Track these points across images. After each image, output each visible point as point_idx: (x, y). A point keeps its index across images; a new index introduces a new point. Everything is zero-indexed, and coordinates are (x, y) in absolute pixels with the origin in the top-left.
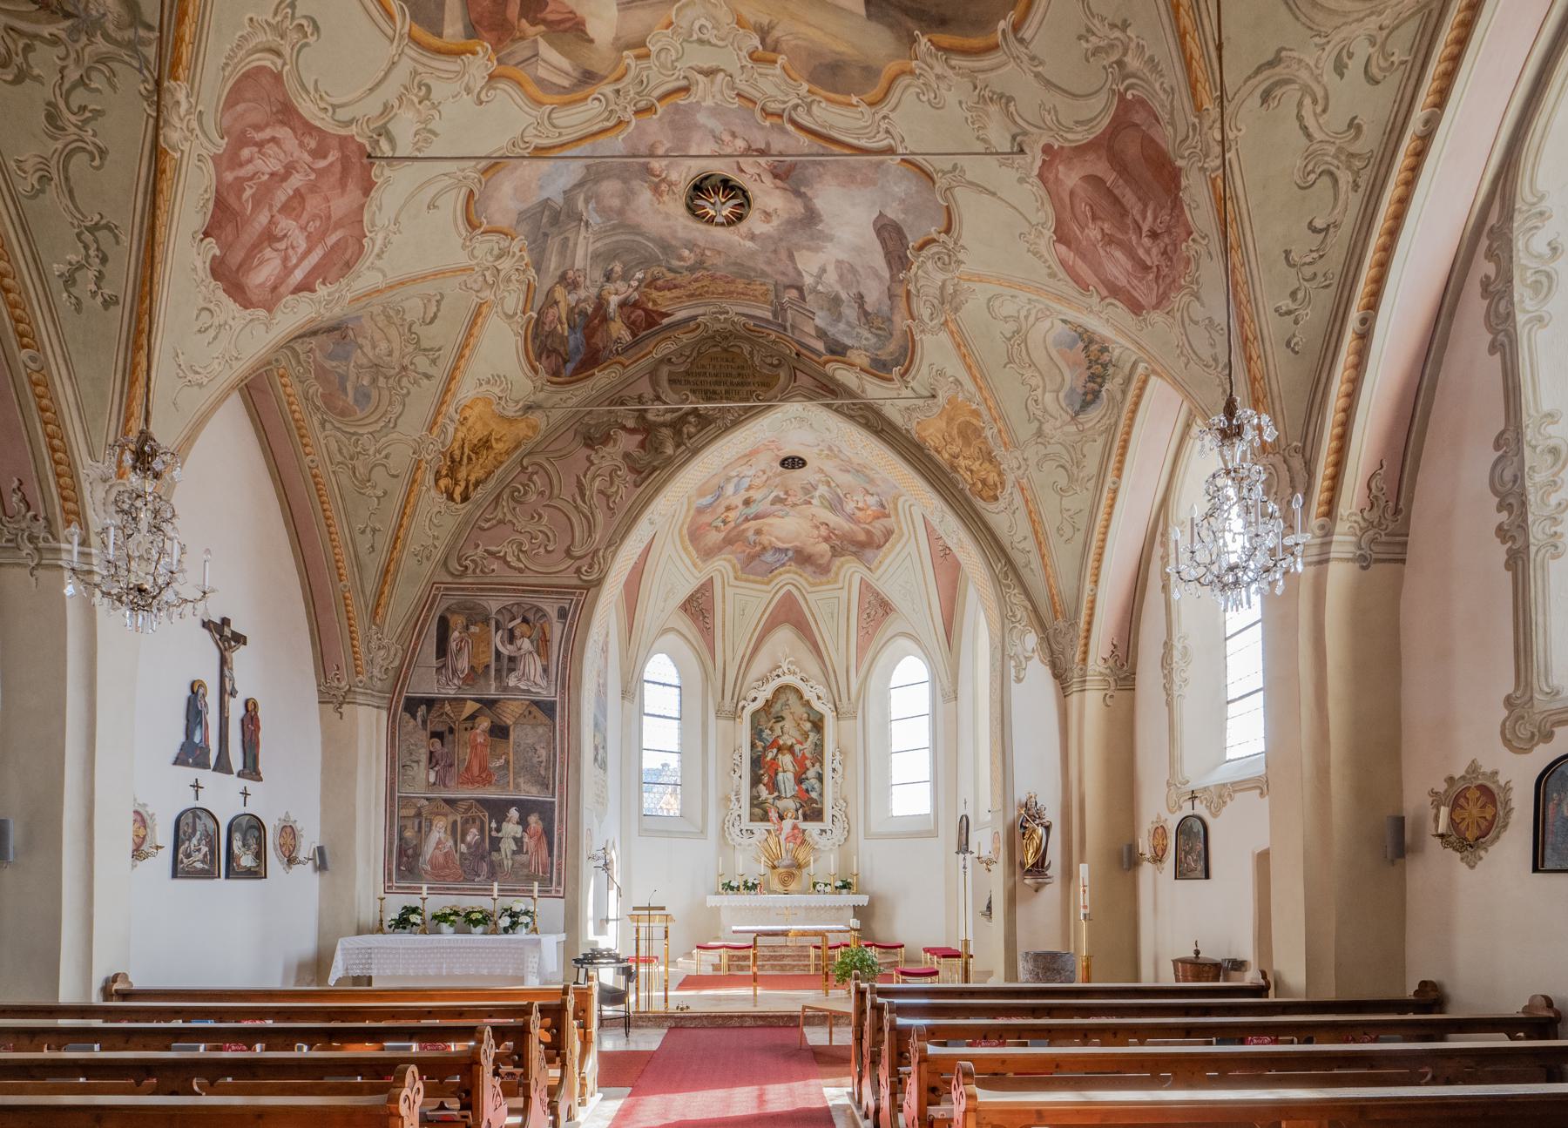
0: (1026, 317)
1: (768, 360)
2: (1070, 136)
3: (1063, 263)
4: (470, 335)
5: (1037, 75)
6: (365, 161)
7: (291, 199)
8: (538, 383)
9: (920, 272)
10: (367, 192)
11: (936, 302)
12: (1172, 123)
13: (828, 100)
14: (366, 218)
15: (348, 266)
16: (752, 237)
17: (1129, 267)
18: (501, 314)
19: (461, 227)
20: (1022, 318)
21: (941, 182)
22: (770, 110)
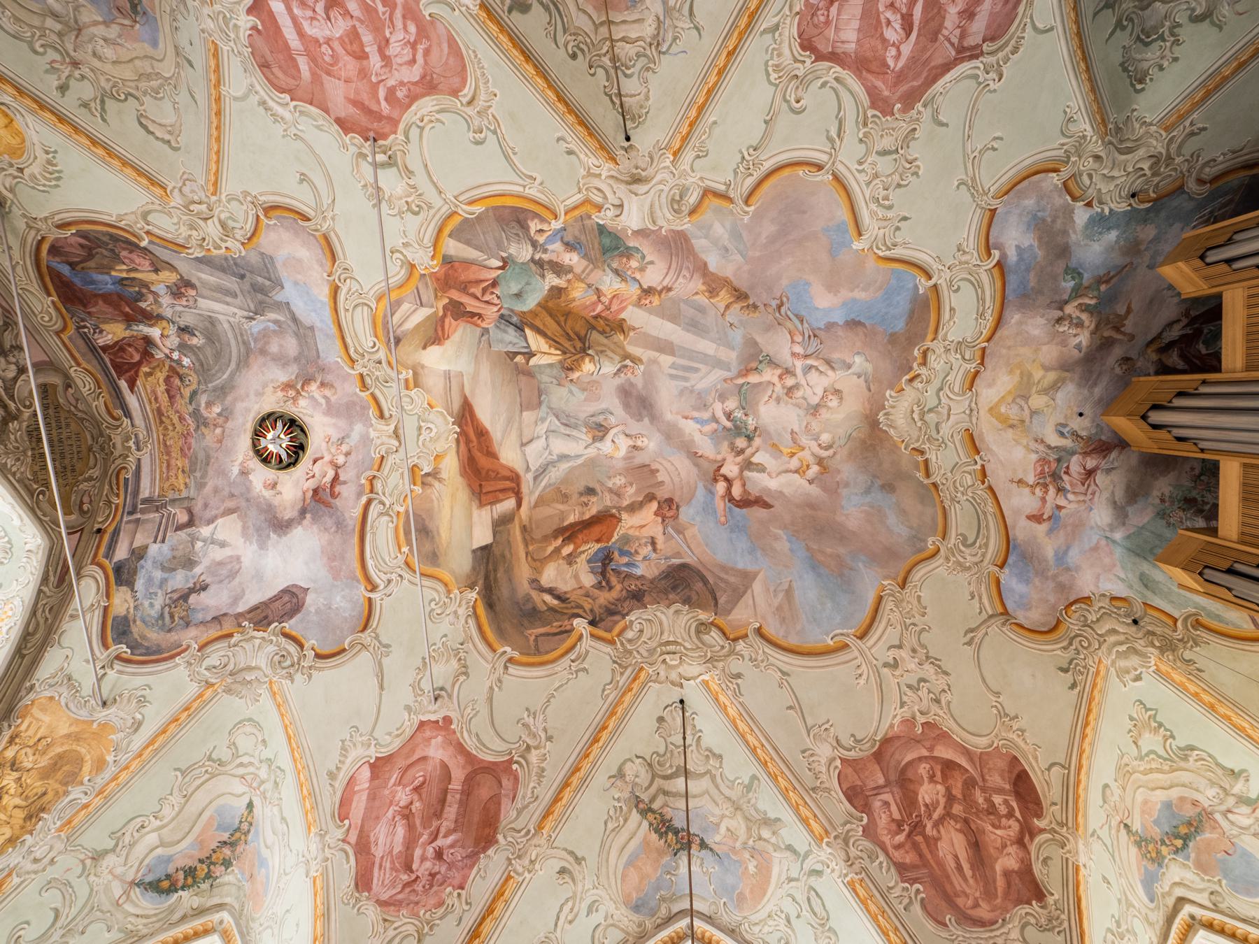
0: (241, 765)
1: (86, 499)
2: (465, 734)
3: (351, 781)
4: (125, 163)
5: (491, 688)
6: (372, 134)
7: (362, 45)
8: (40, 224)
9: (257, 642)
10: (339, 122)
11: (231, 667)
12: (519, 812)
13: (396, 529)
14: (313, 110)
15: (264, 66)
16: (244, 473)
17: (396, 851)
18: (151, 207)
19: (272, 198)
20: (238, 761)
21: (366, 637)
22: (375, 482)
